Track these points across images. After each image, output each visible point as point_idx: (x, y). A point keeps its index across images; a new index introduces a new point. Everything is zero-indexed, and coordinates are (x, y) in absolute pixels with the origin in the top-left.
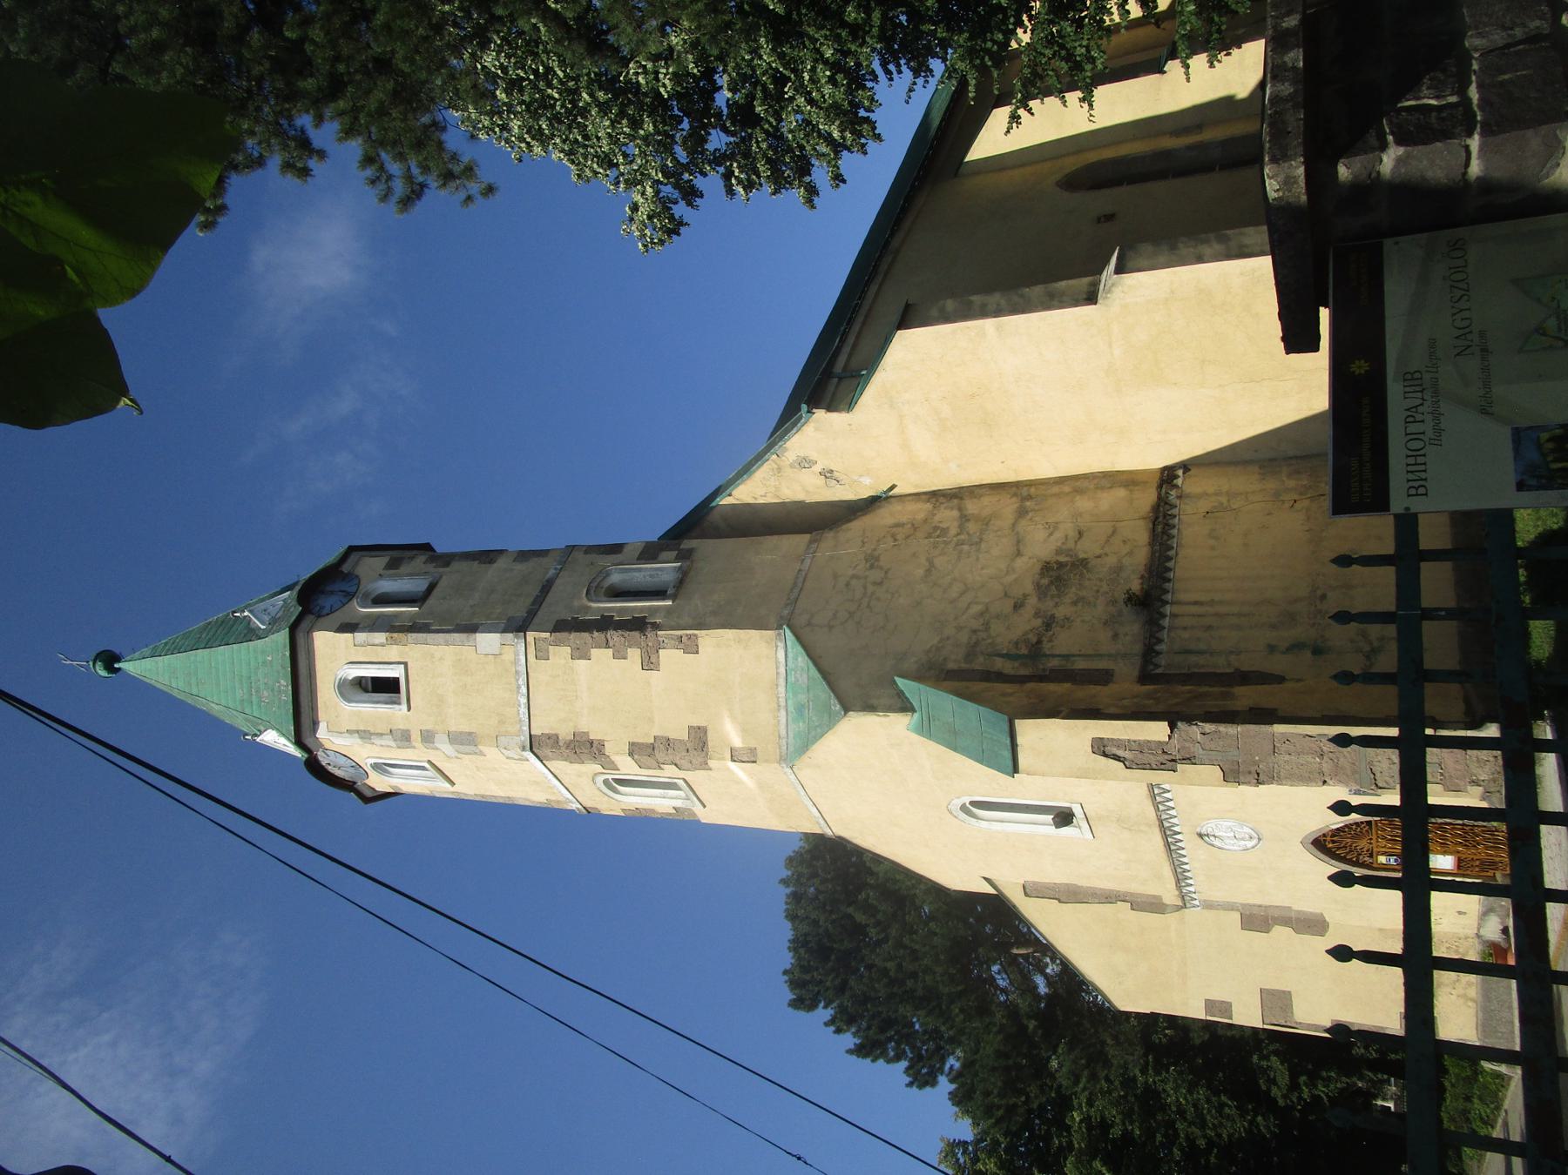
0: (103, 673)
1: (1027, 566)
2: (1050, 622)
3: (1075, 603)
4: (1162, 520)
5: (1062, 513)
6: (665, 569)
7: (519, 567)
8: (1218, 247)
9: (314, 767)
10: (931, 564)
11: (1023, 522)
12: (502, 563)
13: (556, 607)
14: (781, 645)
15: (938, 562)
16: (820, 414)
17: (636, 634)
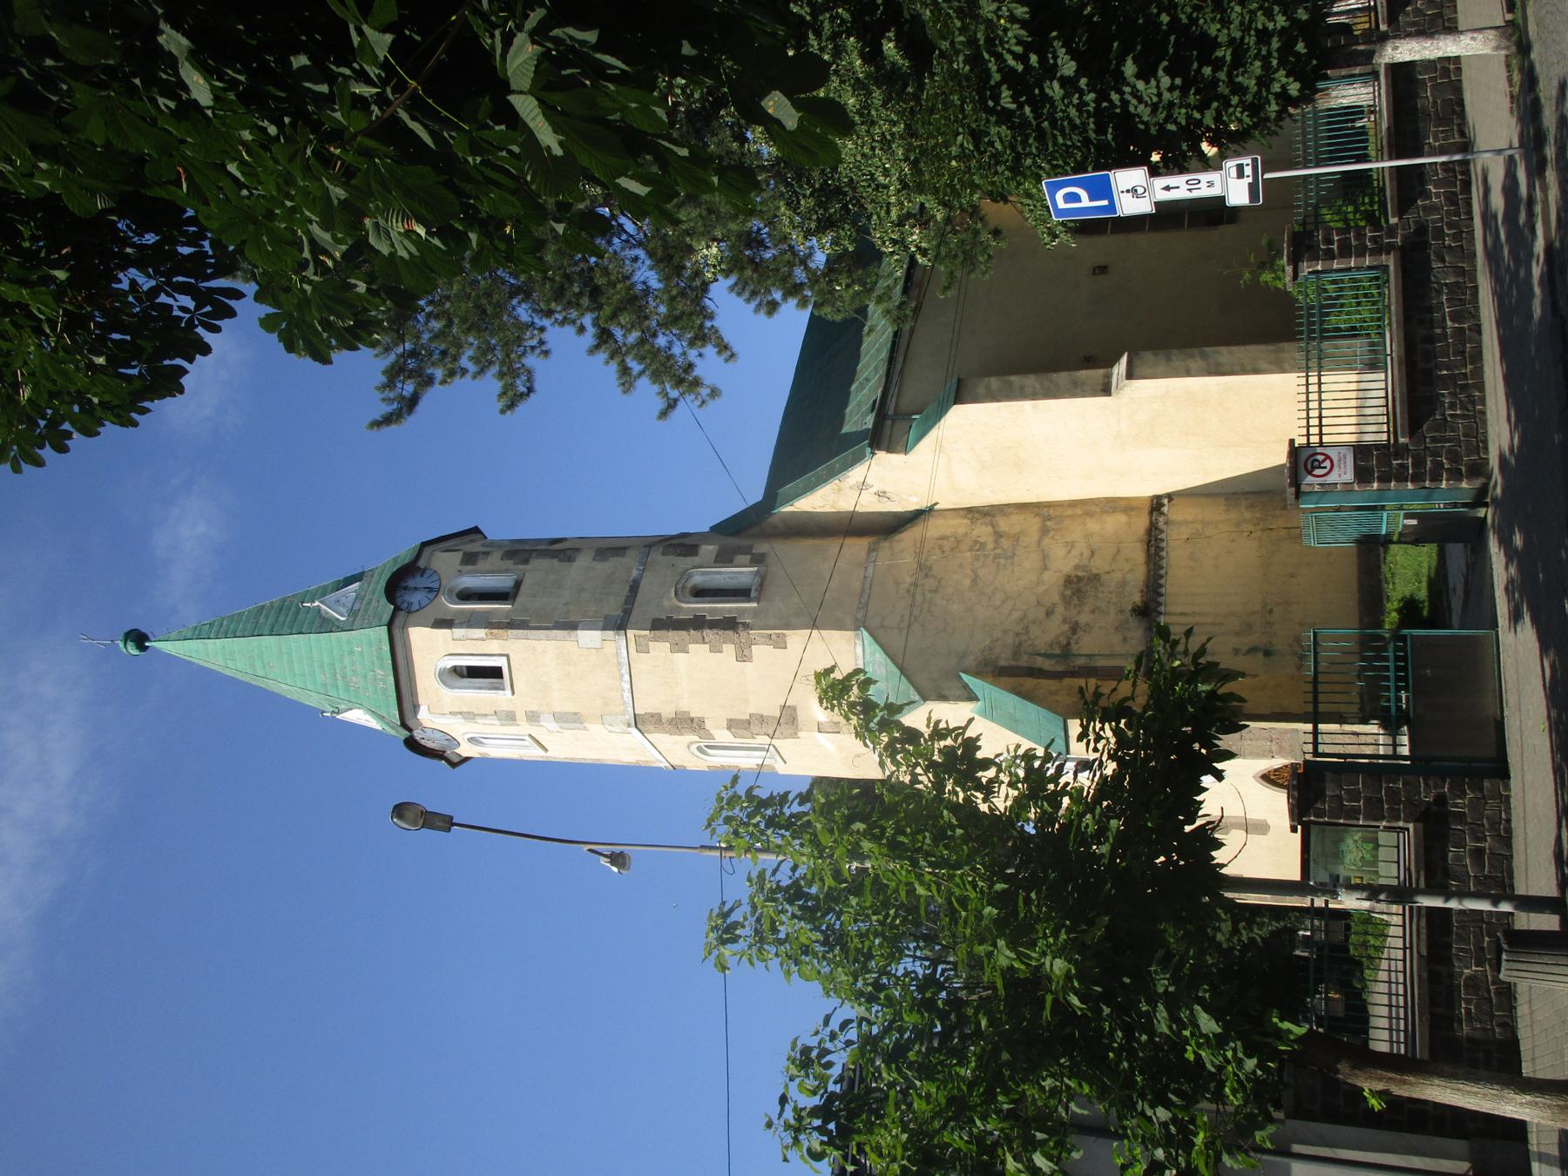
0: (135, 652)
1: (1052, 580)
2: (1075, 628)
3: (1093, 612)
4: (1153, 542)
5: (1076, 532)
6: (740, 573)
7: (600, 566)
8: (1200, 363)
9: (412, 744)
10: (977, 576)
11: (1046, 541)
12: (583, 561)
13: (646, 605)
14: (859, 643)
15: (982, 572)
16: (881, 455)
17: (730, 633)
